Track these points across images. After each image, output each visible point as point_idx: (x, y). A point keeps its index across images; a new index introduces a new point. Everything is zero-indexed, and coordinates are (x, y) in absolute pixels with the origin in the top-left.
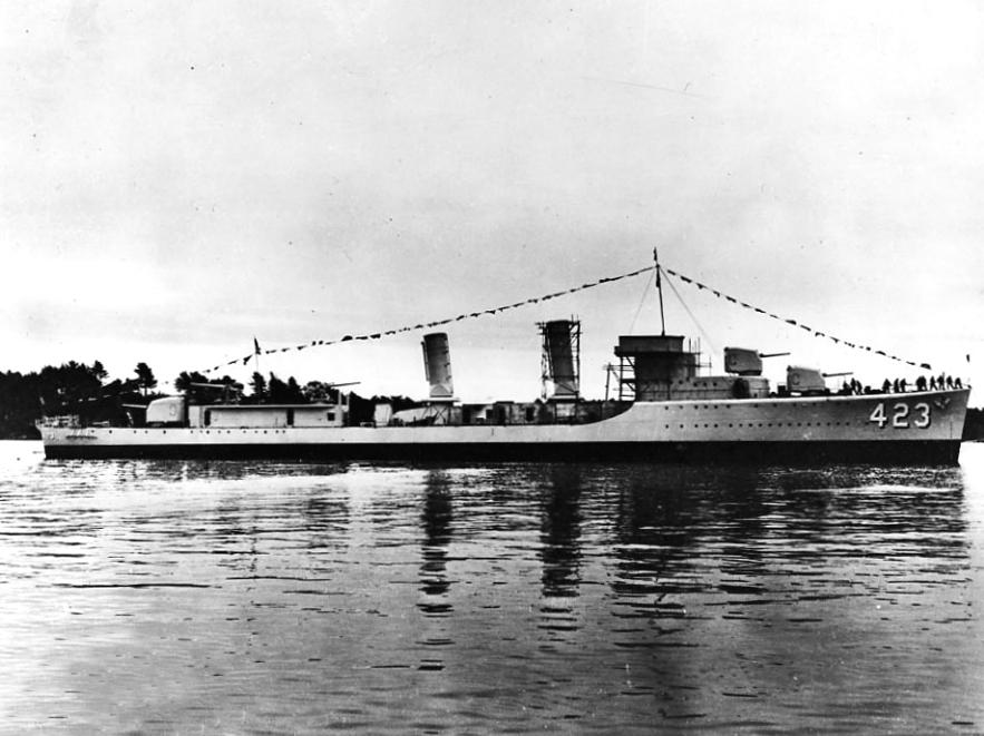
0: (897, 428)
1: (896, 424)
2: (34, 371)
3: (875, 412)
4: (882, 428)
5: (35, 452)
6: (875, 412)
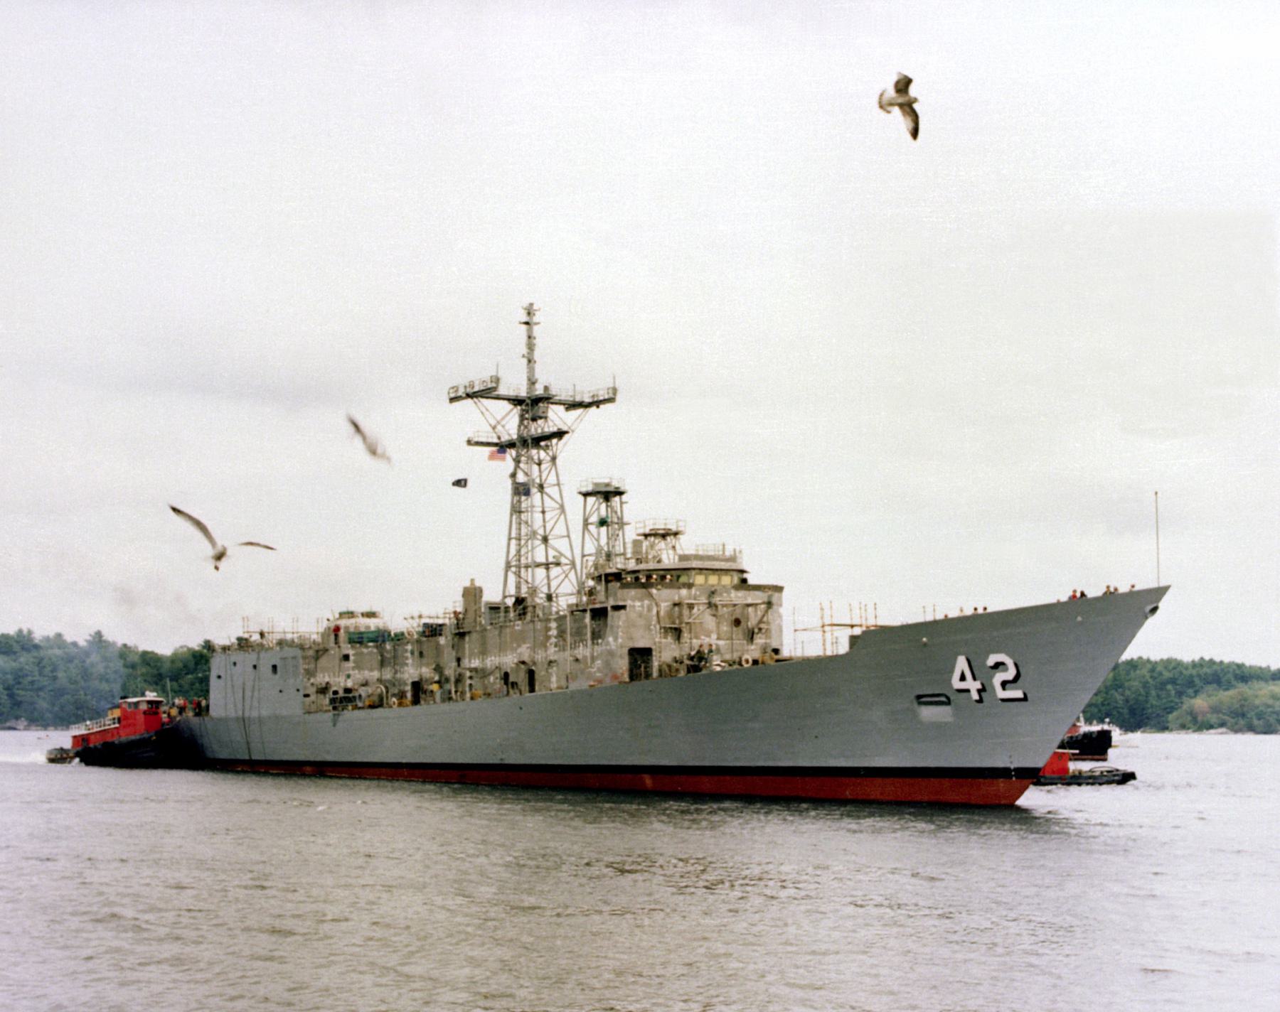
0: (1004, 700)
1: (1002, 694)
2: (116, 640)
3: (957, 675)
4: (980, 701)
5: (1156, 493)
6: (957, 675)
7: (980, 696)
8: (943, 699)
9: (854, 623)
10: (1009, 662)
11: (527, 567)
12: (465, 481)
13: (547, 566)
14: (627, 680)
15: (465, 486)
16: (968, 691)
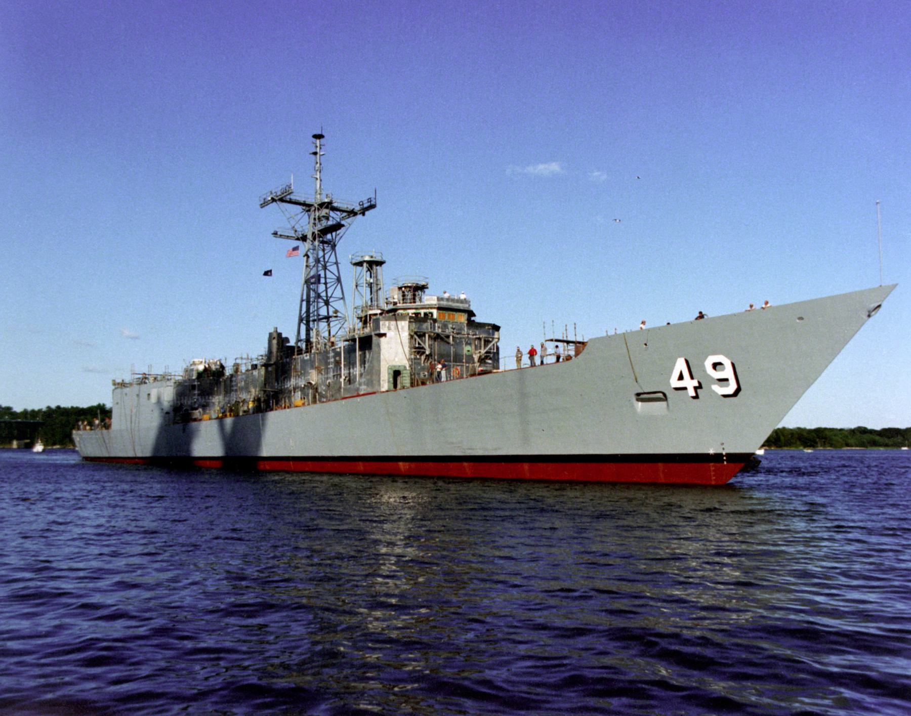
6: (676, 375)
7: (696, 392)
8: (660, 395)
9: (570, 339)
10: (727, 363)
11: (314, 321)
12: (271, 271)
13: (327, 318)
14: (408, 385)
15: (271, 275)
16: (685, 389)
